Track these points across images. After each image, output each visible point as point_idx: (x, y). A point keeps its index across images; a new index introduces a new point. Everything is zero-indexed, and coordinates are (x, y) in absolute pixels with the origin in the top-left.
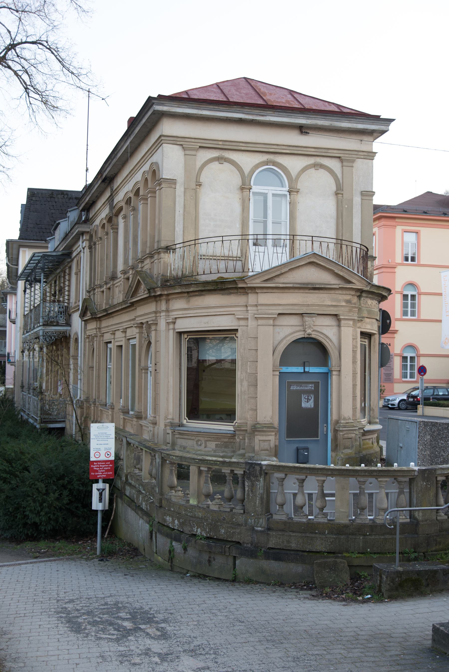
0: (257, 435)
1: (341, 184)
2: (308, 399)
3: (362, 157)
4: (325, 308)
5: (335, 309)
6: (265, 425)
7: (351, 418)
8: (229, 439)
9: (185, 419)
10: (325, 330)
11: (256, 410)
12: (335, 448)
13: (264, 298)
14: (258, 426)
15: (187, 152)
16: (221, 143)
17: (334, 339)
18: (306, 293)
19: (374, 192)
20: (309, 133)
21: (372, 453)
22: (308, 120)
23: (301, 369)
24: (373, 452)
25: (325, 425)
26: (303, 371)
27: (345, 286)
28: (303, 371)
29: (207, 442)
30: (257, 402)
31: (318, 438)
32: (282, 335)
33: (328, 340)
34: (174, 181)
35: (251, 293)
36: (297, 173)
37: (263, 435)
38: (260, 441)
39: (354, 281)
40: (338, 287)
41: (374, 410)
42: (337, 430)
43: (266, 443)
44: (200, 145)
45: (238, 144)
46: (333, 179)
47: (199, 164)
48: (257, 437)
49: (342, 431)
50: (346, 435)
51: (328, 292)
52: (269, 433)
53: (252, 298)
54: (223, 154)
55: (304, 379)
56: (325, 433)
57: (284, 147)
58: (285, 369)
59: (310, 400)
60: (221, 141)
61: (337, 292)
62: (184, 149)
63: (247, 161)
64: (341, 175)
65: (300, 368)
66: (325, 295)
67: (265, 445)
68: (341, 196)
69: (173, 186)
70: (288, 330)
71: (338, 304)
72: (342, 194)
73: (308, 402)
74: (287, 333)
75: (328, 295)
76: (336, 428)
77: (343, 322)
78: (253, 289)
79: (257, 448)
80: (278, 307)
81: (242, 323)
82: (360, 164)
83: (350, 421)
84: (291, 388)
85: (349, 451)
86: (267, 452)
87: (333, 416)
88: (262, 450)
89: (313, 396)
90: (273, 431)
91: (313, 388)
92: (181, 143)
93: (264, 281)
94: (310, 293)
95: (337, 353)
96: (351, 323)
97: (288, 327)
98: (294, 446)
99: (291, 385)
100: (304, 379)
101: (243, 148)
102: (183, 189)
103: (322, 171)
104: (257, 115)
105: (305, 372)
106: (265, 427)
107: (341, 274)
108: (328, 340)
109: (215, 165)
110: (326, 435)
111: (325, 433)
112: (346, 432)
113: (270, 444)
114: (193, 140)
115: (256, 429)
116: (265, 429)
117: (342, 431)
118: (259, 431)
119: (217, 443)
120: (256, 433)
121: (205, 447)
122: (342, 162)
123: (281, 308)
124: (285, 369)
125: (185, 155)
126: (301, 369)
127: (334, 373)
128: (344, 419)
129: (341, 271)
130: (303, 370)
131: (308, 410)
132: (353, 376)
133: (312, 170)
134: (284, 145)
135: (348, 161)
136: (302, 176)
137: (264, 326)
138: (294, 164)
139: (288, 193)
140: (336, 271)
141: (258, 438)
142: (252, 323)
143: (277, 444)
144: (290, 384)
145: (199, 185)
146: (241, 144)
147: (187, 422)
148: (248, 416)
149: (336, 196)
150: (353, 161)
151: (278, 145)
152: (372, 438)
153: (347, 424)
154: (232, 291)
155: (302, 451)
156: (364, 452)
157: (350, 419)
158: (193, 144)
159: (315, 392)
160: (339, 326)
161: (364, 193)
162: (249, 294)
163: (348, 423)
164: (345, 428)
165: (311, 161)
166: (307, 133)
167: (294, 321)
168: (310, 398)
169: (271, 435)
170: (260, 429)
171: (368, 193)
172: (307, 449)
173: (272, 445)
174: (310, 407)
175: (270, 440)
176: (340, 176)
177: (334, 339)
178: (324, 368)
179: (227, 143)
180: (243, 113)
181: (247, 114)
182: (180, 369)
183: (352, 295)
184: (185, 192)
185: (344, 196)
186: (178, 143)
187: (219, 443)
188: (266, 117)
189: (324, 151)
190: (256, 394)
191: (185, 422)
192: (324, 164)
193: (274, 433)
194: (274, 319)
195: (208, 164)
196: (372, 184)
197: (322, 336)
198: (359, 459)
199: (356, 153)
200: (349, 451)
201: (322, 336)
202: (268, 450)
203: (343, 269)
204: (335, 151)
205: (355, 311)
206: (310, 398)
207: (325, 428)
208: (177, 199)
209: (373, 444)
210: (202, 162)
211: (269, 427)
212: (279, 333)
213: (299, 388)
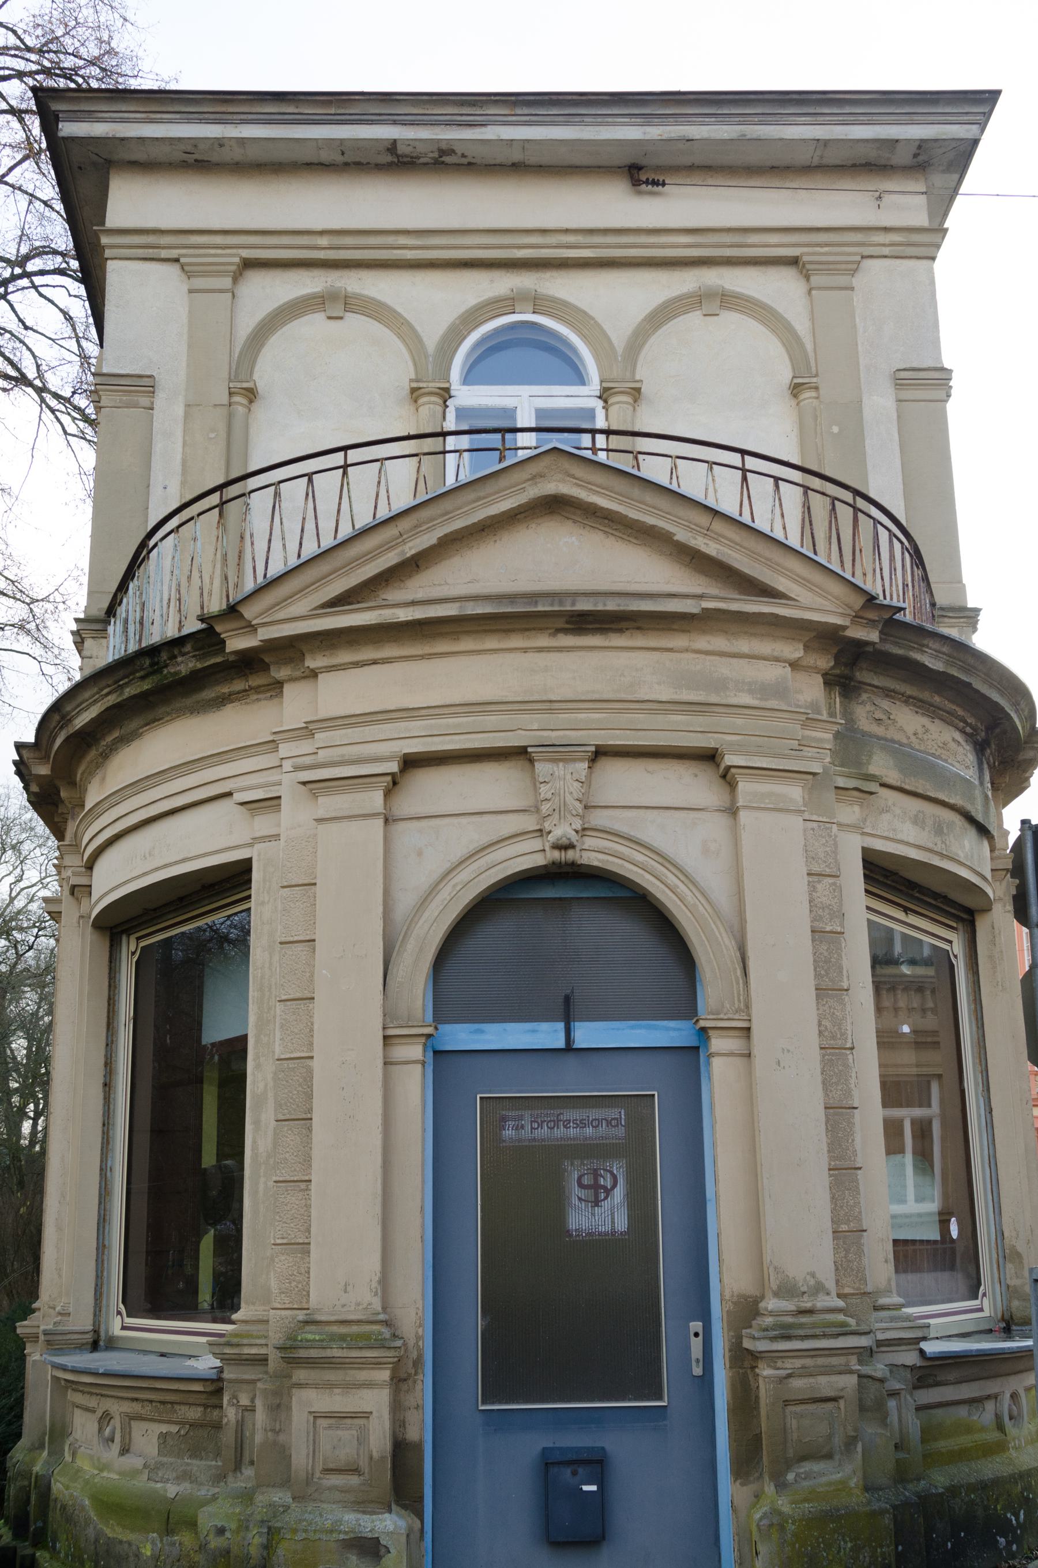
0: (300, 1386)
1: (811, 354)
2: (596, 1187)
3: (886, 251)
4: (641, 719)
5: (699, 721)
6: (343, 1330)
7: (831, 1285)
8: (206, 1406)
9: (119, 1313)
10: (662, 831)
11: (304, 1248)
12: (747, 1460)
13: (340, 690)
14: (310, 1334)
15: (200, 283)
16: (324, 241)
17: (713, 876)
18: (540, 650)
19: (951, 371)
20: (664, 184)
21: (996, 1482)
22: (648, 129)
23: (548, 1035)
24: (1006, 1471)
25: (696, 1326)
26: (561, 1044)
27: (734, 607)
28: (561, 1044)
29: (134, 1424)
30: (308, 1207)
31: (660, 1398)
32: (433, 865)
33: (672, 879)
34: (146, 381)
35: (292, 679)
36: (630, 331)
37: (330, 1386)
38: (316, 1416)
39: (782, 584)
40: (695, 610)
41: (1019, 1255)
42: (755, 1356)
43: (347, 1433)
44: (246, 254)
45: (390, 240)
46: (779, 344)
47: (247, 323)
48: (310, 1394)
49: (773, 1357)
50: (797, 1383)
51: (653, 643)
52: (363, 1375)
53: (297, 703)
54: (338, 284)
55: (572, 1081)
56: (697, 1371)
57: (571, 239)
58: (462, 1036)
59: (608, 1192)
60: (322, 233)
61: (702, 642)
62: (188, 272)
63: (434, 301)
64: (808, 324)
65: (545, 1026)
66: (640, 659)
67: (338, 1443)
68: (814, 394)
69: (144, 401)
70: (467, 836)
71: (713, 699)
72: (817, 388)
73: (596, 1203)
74: (459, 852)
75: (656, 655)
76: (747, 1344)
77: (745, 787)
78: (292, 649)
79: (300, 1458)
80: (403, 725)
81: (263, 824)
82: (877, 274)
83: (822, 1302)
84: (508, 1133)
85: (826, 1474)
86: (354, 1480)
87: (729, 1276)
88: (327, 1471)
89: (619, 1168)
90: (377, 1364)
91: (621, 1131)
92: (174, 253)
93: (324, 606)
94: (560, 649)
95: (729, 945)
96: (794, 792)
97: (464, 820)
98: (531, 1445)
99: (504, 1119)
100: (572, 1081)
101: (409, 255)
102: (179, 410)
103: (731, 319)
104: (448, 124)
105: (569, 1048)
106: (343, 1338)
107: (711, 548)
108: (672, 879)
109: (312, 327)
110: (706, 1380)
111: (697, 1371)
112: (798, 1363)
113: (362, 1440)
114: (218, 240)
115: (306, 1352)
116: (336, 1353)
117: (773, 1357)
118: (311, 1363)
119: (164, 1428)
120: (301, 1375)
121: (125, 1451)
122: (807, 278)
123: (416, 727)
124: (462, 1036)
125: (191, 291)
126: (548, 1035)
127: (718, 1043)
128: (787, 1290)
129: (706, 532)
130: (562, 1036)
131: (600, 1246)
132: (827, 1065)
133: (694, 319)
134: (567, 231)
135: (829, 268)
136: (652, 340)
137: (344, 824)
138: (617, 300)
139: (599, 404)
140: (681, 535)
141: (309, 1400)
142: (295, 815)
143: (421, 1428)
144: (496, 1110)
145: (251, 394)
146: (402, 240)
147: (123, 1328)
148: (274, 1284)
149: (794, 402)
150: (854, 270)
151: (544, 232)
152: (995, 1397)
153: (804, 1319)
154: (225, 689)
155: (567, 1472)
156: (940, 1479)
157: (819, 1288)
158: (219, 251)
159: (637, 1151)
160: (732, 811)
161: (903, 374)
162: (287, 688)
163: (810, 1312)
164: (788, 1338)
165: (685, 282)
166: (655, 183)
167: (492, 787)
168: (606, 1181)
169: (369, 1385)
170: (313, 1353)
171: (921, 375)
172: (596, 1464)
173: (379, 1439)
174: (608, 1228)
175: (367, 1415)
176: (802, 326)
177: (713, 876)
178: (672, 1024)
179: (349, 241)
180: (395, 123)
181: (412, 124)
182: (108, 1086)
183: (794, 665)
184: (187, 416)
185: (821, 391)
186: (164, 254)
187: (174, 1429)
188: (483, 129)
189: (728, 239)
190: (307, 1161)
191: (116, 1328)
192: (738, 289)
193: (385, 1375)
194: (394, 783)
195: (284, 324)
196: (936, 343)
197: (639, 858)
198: (887, 1520)
199: (858, 237)
200: (826, 1474)
201: (639, 858)
202: (356, 1471)
203: (718, 526)
204: (774, 238)
205: (821, 740)
206: (606, 1181)
207: (696, 1346)
208: (158, 447)
209: (1001, 1427)
210: (260, 315)
211: (372, 1338)
212: (420, 854)
213: (543, 1132)
